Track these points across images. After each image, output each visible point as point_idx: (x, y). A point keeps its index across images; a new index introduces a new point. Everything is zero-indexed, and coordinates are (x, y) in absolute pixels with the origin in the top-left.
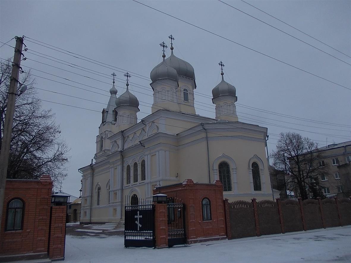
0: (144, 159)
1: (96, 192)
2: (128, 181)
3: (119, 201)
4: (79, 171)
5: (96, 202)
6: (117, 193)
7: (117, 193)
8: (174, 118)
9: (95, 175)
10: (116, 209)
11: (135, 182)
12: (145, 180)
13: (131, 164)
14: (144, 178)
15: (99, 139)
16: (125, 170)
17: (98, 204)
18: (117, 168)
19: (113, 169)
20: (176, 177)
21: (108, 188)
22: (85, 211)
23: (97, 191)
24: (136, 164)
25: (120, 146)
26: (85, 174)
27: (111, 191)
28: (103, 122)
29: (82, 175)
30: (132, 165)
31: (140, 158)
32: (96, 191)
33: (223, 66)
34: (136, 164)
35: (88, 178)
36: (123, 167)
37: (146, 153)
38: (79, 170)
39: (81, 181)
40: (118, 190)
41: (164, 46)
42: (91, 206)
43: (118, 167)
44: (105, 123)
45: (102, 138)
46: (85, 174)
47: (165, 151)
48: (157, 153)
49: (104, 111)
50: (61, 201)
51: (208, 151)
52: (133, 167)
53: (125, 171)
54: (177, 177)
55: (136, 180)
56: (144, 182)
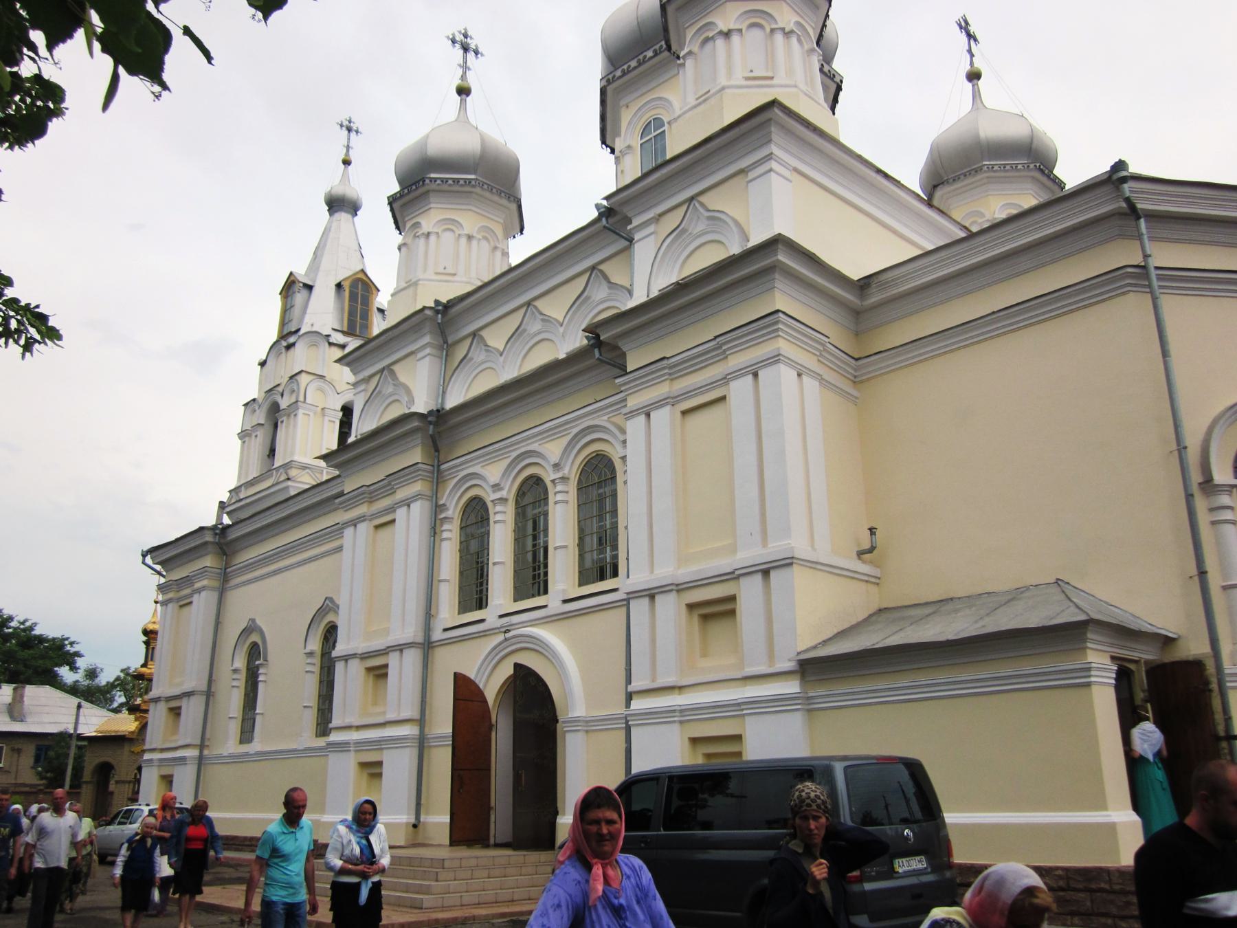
0: (615, 453)
1: (235, 671)
2: (474, 593)
3: (407, 713)
4: (148, 560)
5: (234, 728)
6: (392, 672)
7: (386, 666)
8: (849, 159)
9: (233, 582)
10: (380, 764)
11: (465, 612)
12: (546, 592)
13: (496, 487)
14: (600, 564)
15: (261, 417)
16: (451, 535)
17: (247, 734)
18: (339, 549)
19: (362, 527)
20: (860, 554)
21: (315, 645)
22: (166, 771)
23: (240, 663)
24: (532, 496)
25: (416, 394)
26: (177, 575)
27: (346, 658)
28: (283, 337)
29: (163, 580)
30: (566, 471)
31: (509, 465)
32: (310, 647)
33: (471, 55)
34: (532, 496)
35: (191, 595)
36: (438, 508)
37: (633, 402)
38: (144, 556)
39: (146, 632)
40: (400, 648)
41: (466, 49)
42: (202, 747)
43: (401, 514)
44: (292, 340)
45: (275, 409)
46: (177, 575)
47: (799, 375)
48: (740, 389)
49: (293, 282)
50: (37, 631)
51: (1165, 354)
52: (510, 509)
54: (872, 550)
55: (532, 577)
56: (483, 621)
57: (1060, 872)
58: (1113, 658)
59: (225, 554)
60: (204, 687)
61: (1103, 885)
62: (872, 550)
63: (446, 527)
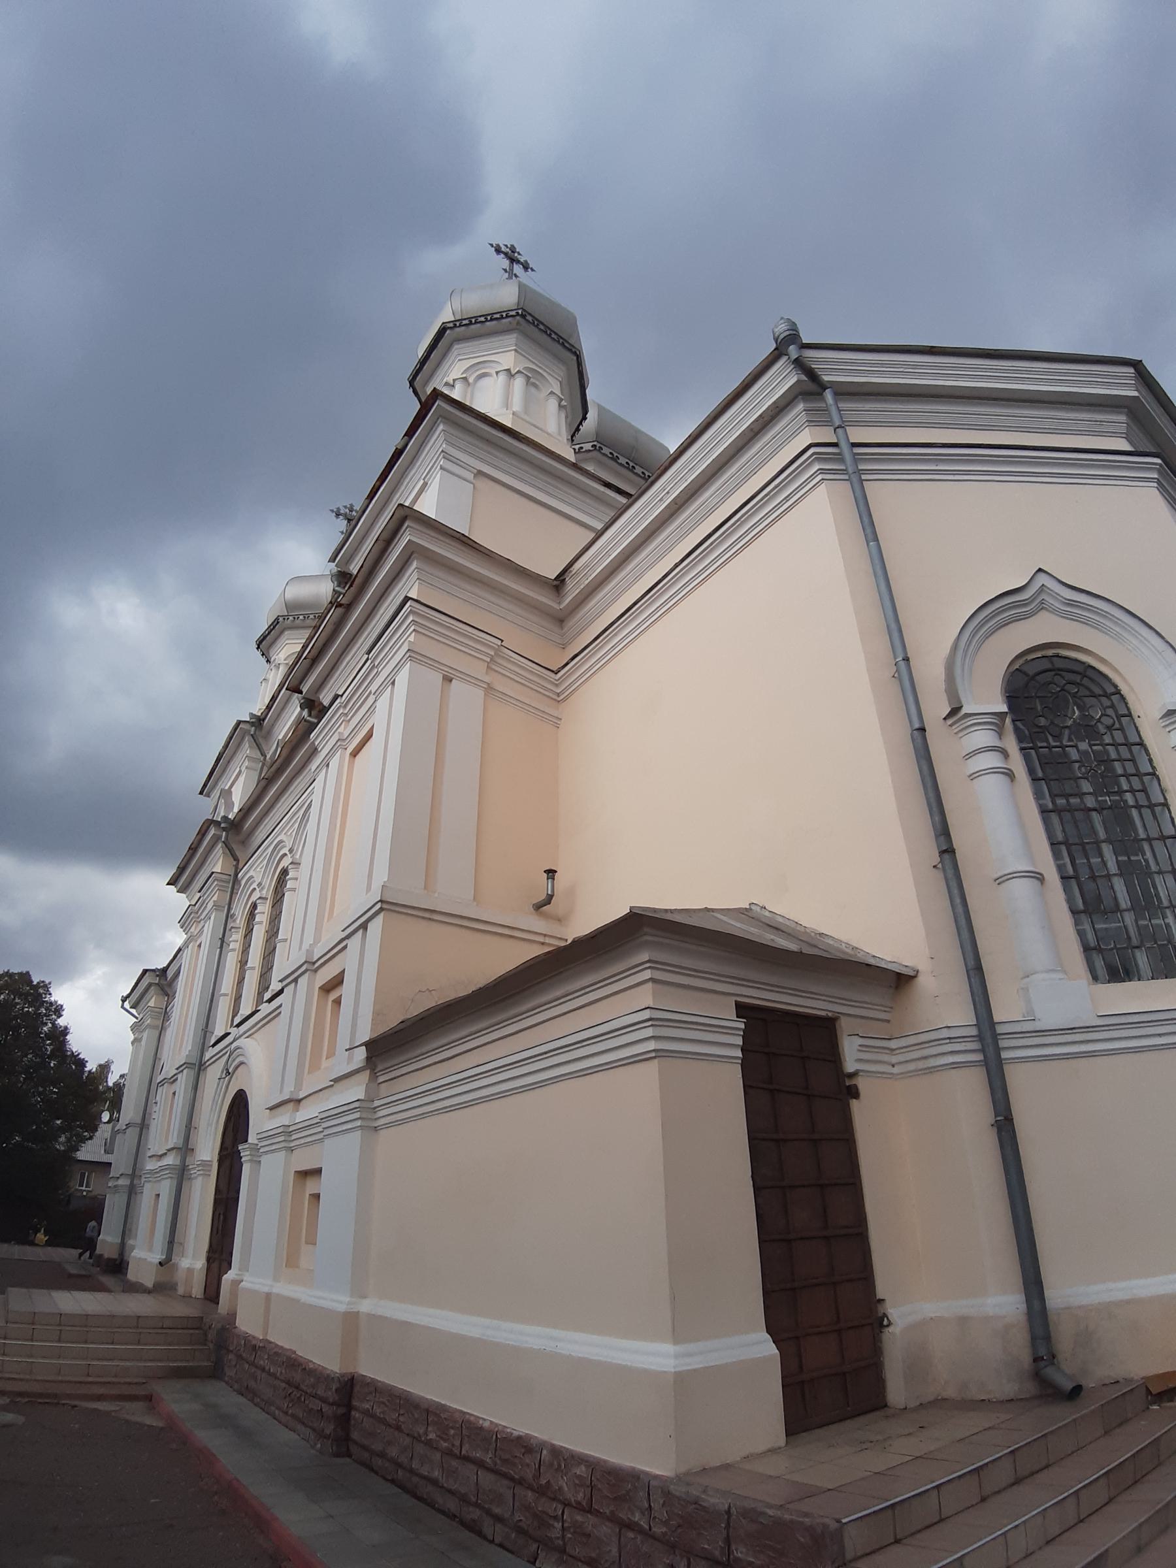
20: (538, 907)
47: (448, 680)
53: (232, 946)
54: (549, 899)
57: (581, 1470)
58: (742, 1010)
59: (167, 995)
60: (139, 1121)
61: (637, 1517)
62: (549, 899)
63: (234, 937)
